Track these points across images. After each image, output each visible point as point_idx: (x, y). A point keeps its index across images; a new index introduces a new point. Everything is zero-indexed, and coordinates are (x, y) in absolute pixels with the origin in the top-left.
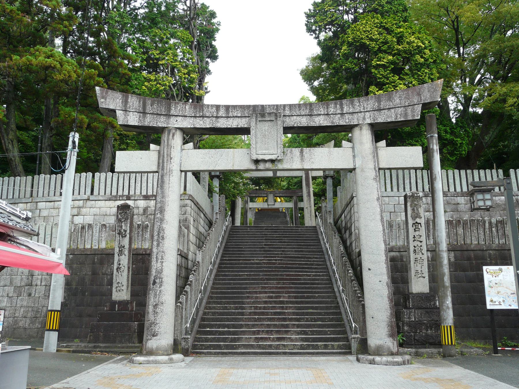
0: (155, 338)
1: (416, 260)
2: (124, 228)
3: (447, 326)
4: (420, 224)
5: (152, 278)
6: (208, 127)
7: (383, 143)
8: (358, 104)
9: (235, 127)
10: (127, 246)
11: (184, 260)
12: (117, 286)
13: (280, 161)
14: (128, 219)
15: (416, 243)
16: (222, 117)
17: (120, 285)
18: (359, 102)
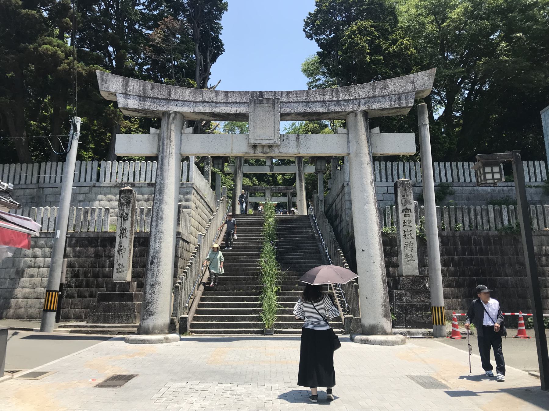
0: (151, 317)
2: (126, 211)
3: (438, 307)
5: (150, 258)
6: (207, 111)
7: (377, 129)
8: (353, 91)
10: (129, 229)
12: (118, 267)
14: (130, 203)
16: (221, 103)
17: (121, 266)
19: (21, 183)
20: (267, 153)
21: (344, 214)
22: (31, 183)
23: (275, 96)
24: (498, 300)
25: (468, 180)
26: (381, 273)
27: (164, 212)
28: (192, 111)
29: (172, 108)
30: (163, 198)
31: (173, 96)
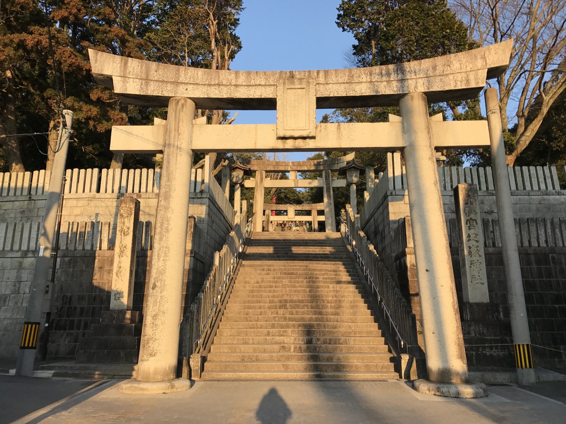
1: (472, 263)
2: (126, 224)
3: (523, 345)
4: (476, 220)
6: (225, 97)
9: (258, 97)
11: (199, 264)
13: (313, 138)
19: (10, 195)
21: (386, 229)
22: (21, 195)
25: (536, 188)
26: (452, 301)
31: (182, 79)
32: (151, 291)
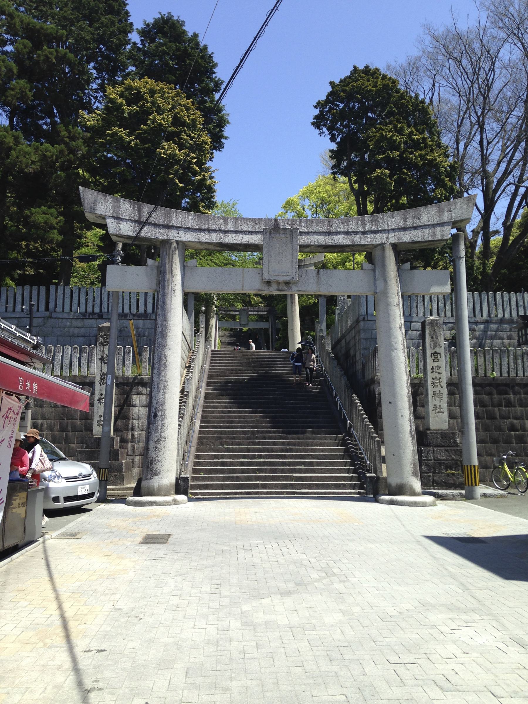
0: (156, 477)
4: (440, 354)
6: (215, 241)
9: (245, 243)
12: (99, 419)
15: (435, 375)
18: (383, 219)
20: (283, 291)
23: (292, 225)
24: (266, 413)
27: (168, 359)
28: (197, 240)
29: (174, 235)
30: (166, 342)
31: (174, 222)
32: (153, 419)
